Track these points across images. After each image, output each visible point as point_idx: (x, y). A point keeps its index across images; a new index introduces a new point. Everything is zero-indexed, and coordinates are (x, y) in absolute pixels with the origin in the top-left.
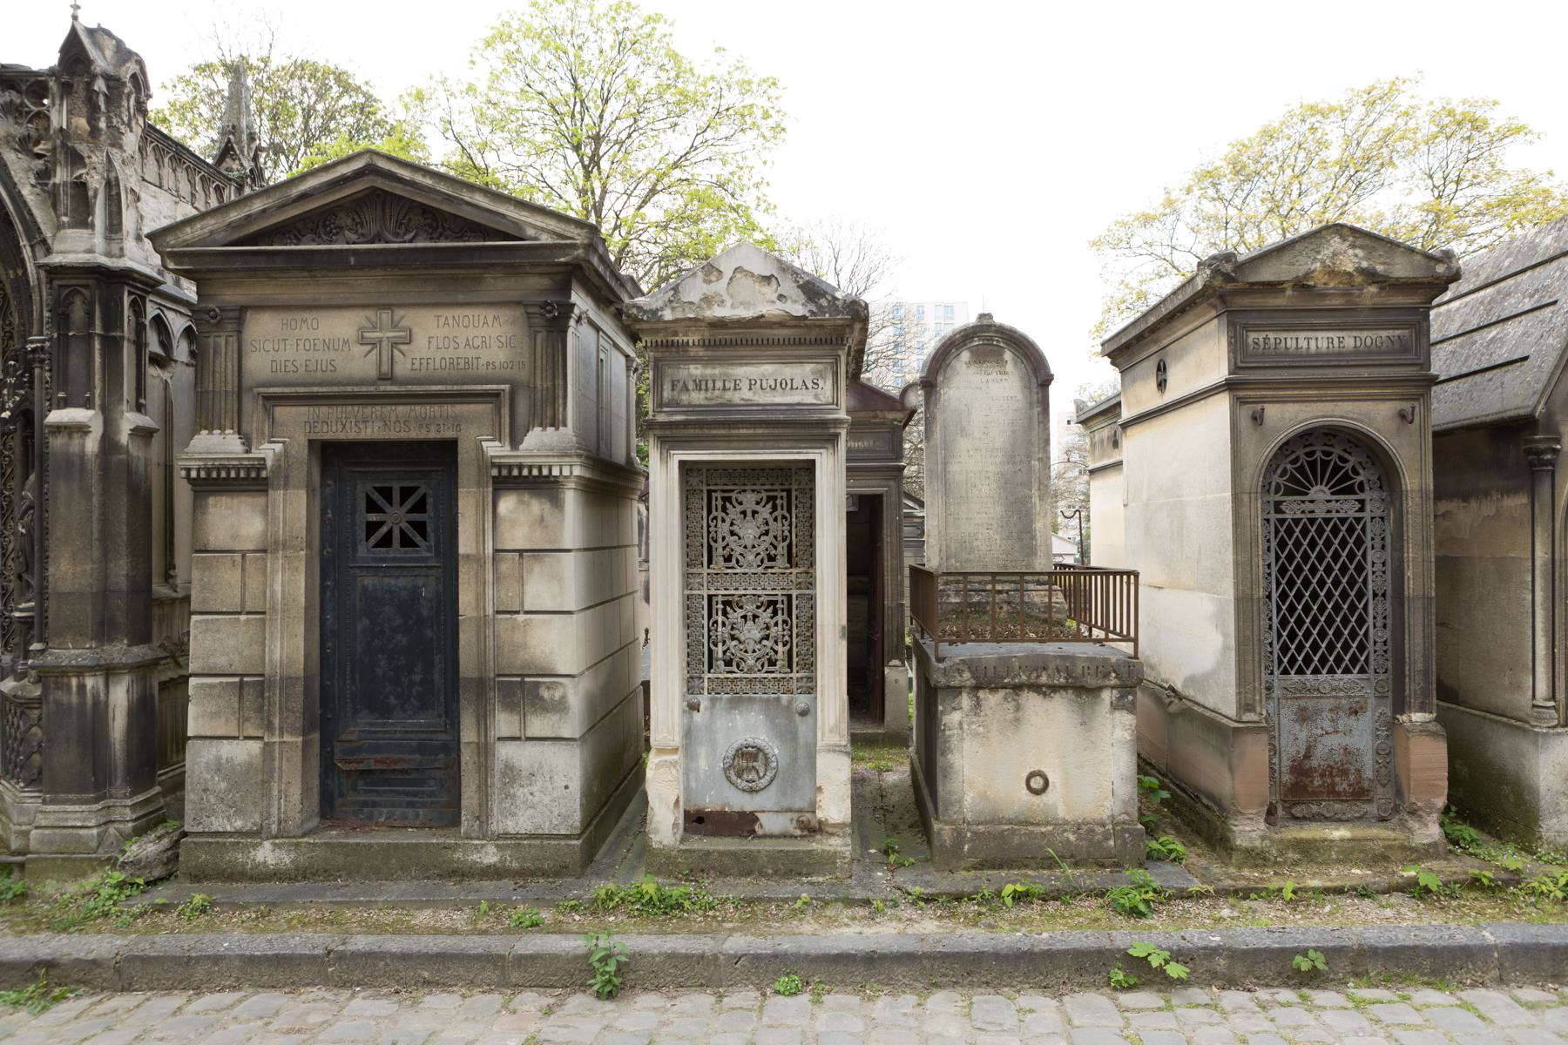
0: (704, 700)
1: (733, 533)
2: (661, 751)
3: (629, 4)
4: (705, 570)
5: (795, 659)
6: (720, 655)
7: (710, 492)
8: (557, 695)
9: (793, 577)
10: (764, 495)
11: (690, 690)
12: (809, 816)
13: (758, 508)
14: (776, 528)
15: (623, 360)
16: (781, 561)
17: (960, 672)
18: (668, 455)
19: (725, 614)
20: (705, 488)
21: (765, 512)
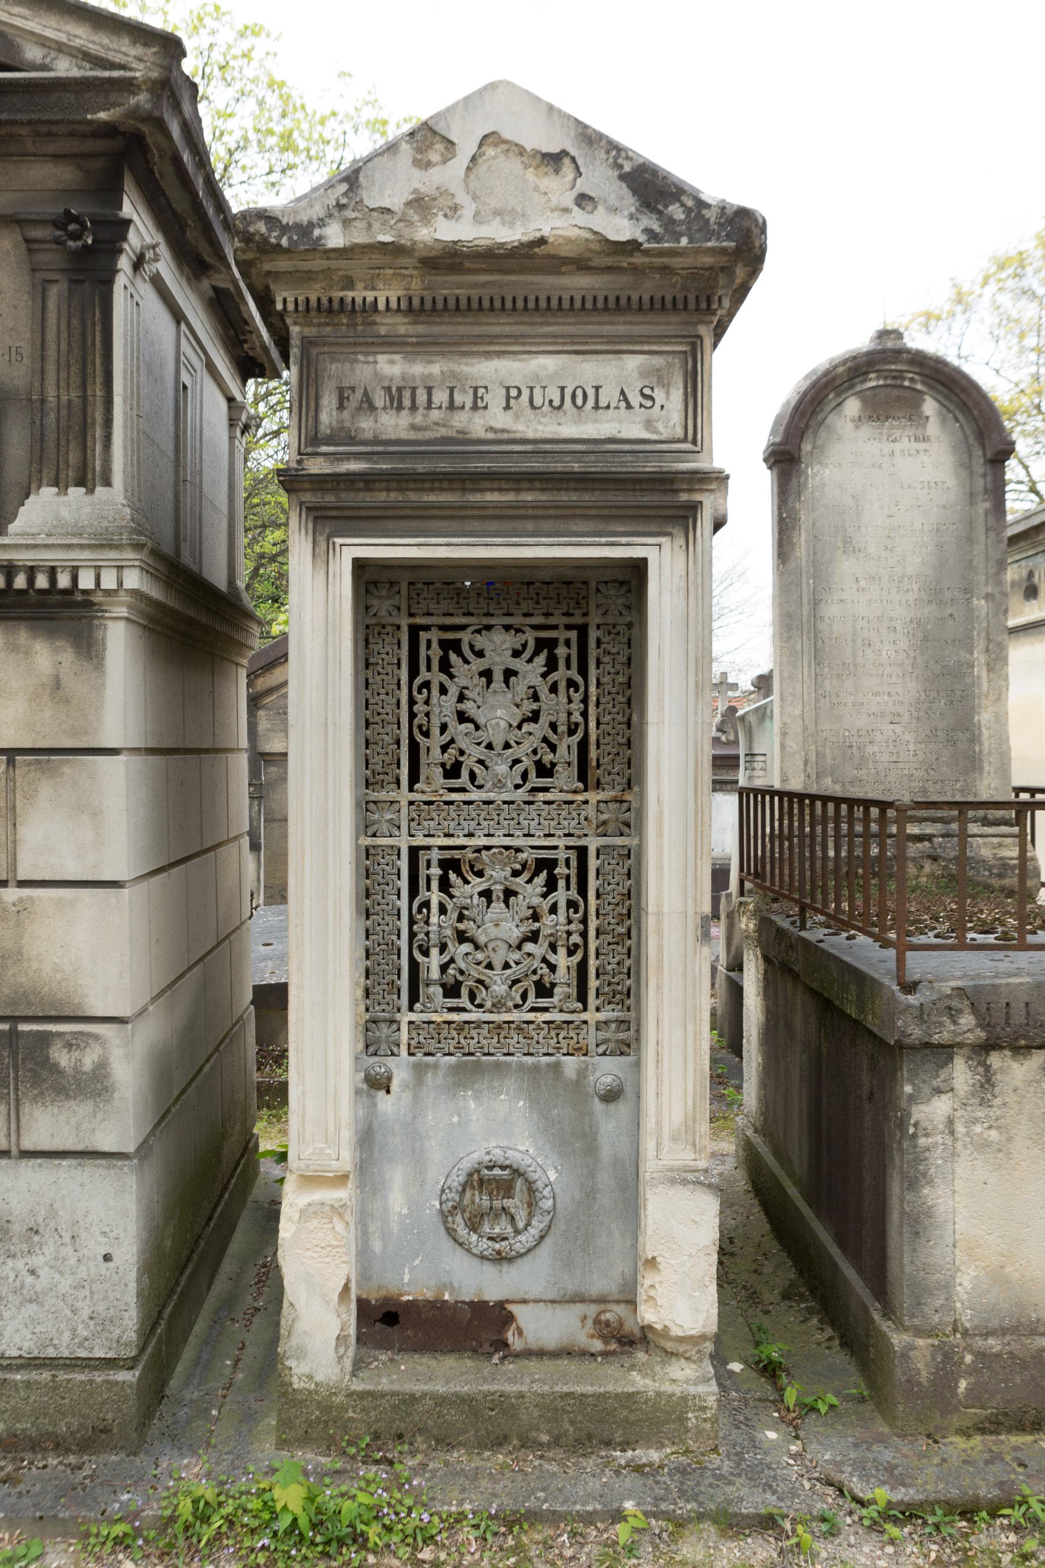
0: (400, 1069)
1: (463, 717)
2: (311, 1180)
3: (217, 8)
4: (404, 795)
5: (593, 983)
6: (435, 974)
7: (414, 631)
8: (89, 1060)
9: (590, 811)
10: (530, 637)
11: (371, 1047)
12: (620, 1310)
13: (518, 664)
14: (554, 707)
15: (223, 405)
16: (565, 777)
17: (953, 1014)
18: (330, 547)
19: (445, 885)
20: (405, 622)
21: (531, 672)
